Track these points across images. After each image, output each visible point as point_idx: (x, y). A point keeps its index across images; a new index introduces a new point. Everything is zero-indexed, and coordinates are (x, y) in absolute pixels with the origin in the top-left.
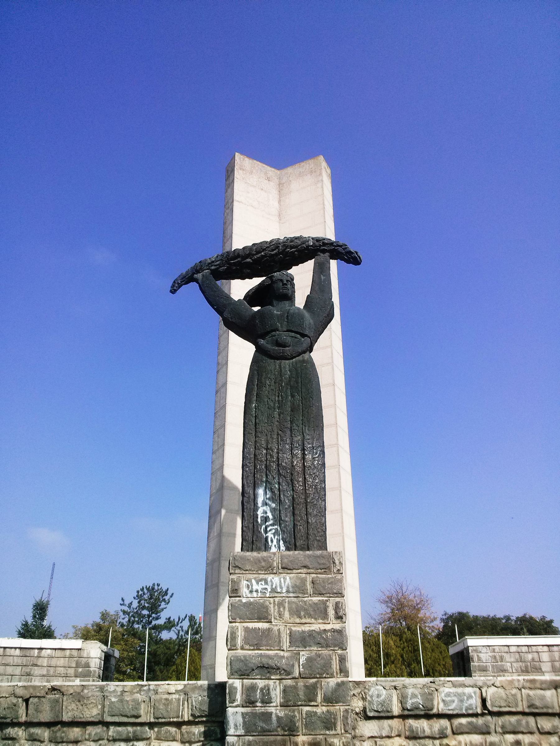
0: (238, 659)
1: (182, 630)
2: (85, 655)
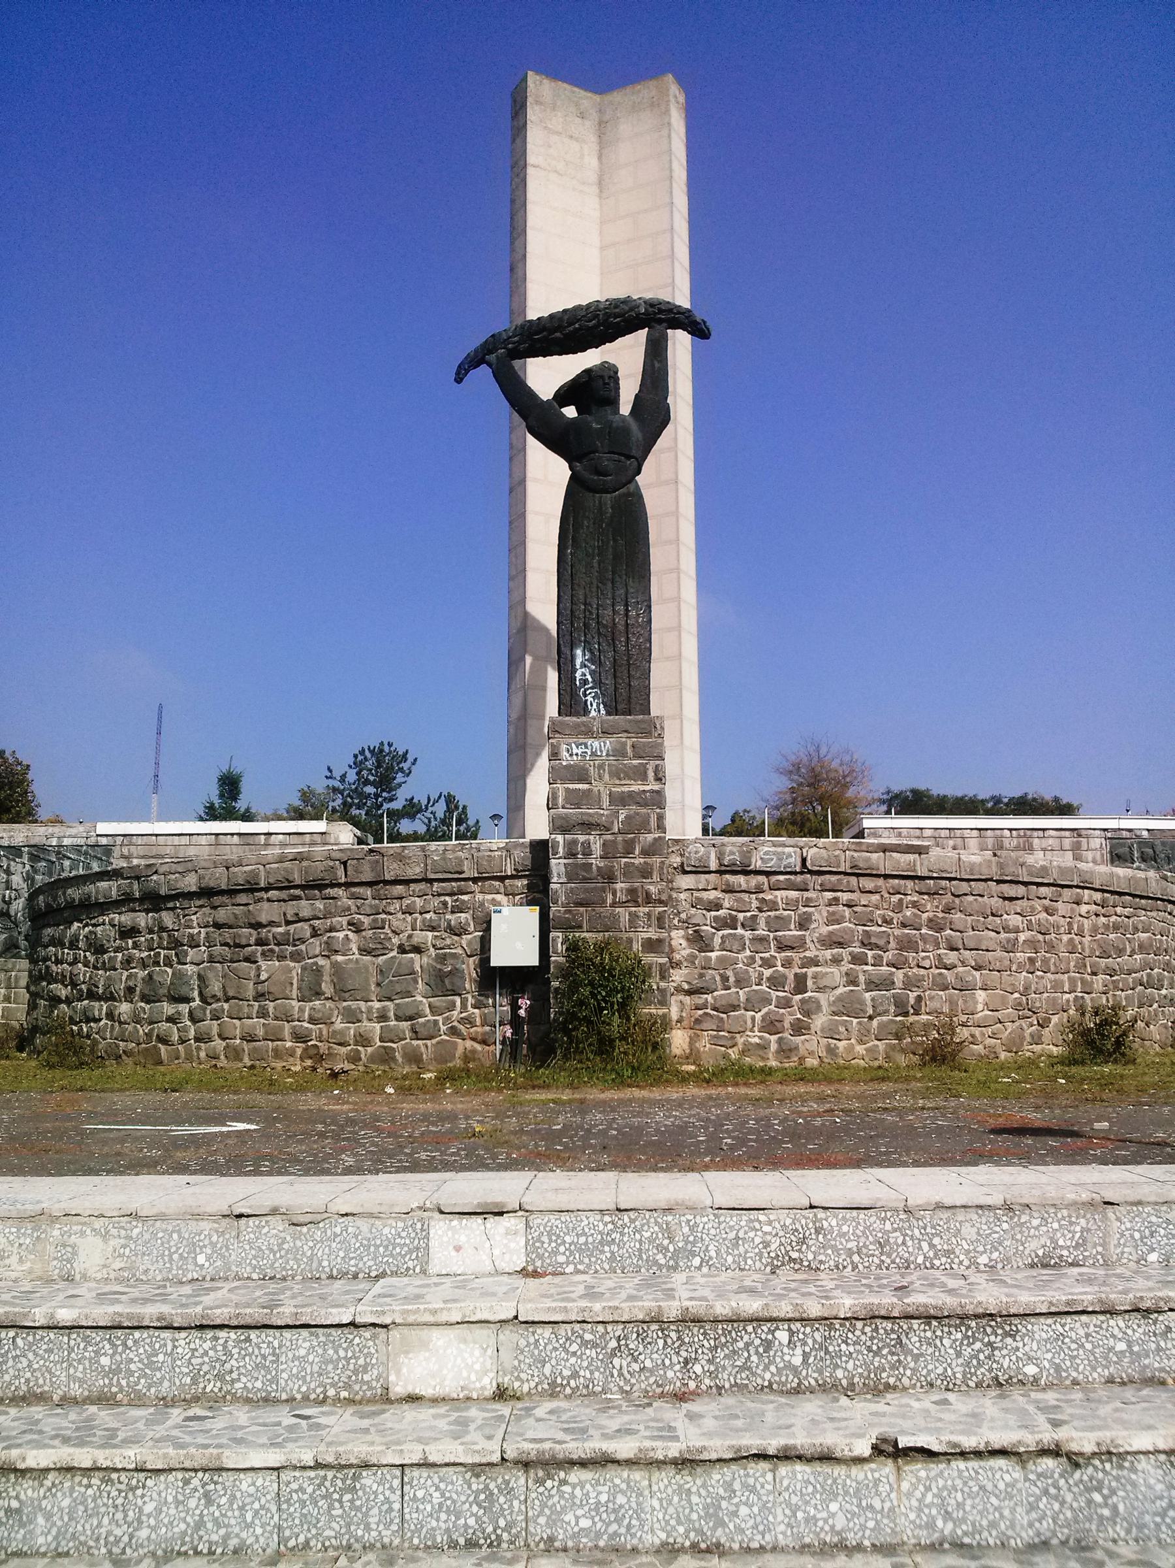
0: (560, 817)
1: (435, 819)
2: (332, 841)
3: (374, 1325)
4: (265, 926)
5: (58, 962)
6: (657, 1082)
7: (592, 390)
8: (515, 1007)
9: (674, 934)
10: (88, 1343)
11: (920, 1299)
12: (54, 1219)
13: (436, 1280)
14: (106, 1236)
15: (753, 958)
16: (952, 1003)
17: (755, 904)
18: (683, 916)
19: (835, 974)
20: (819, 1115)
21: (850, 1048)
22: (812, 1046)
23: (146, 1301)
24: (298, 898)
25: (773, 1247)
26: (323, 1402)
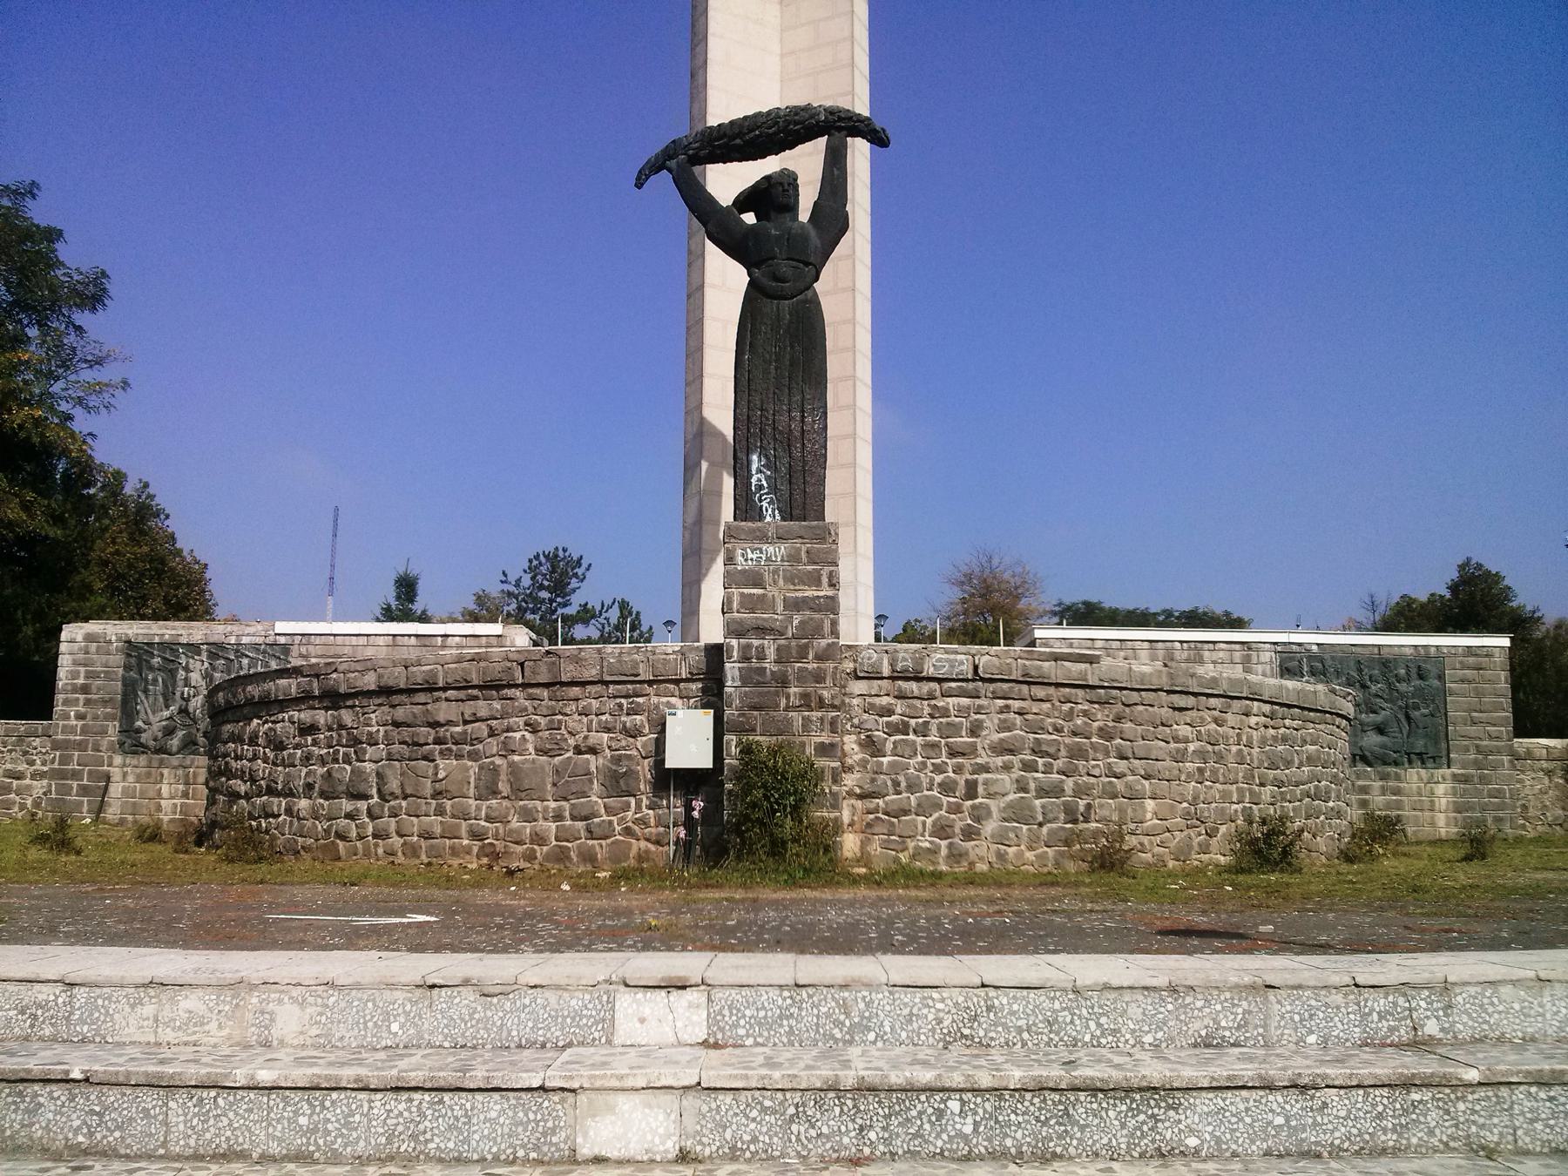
3: (563, 1089)
4: (443, 725)
5: (237, 758)
6: (830, 883)
7: (771, 197)
8: (689, 808)
9: (846, 738)
10: (287, 1104)
11: (1088, 1073)
12: (253, 987)
13: (620, 1050)
14: (302, 1004)
15: (924, 764)
16: (1122, 811)
17: (927, 710)
18: (856, 721)
19: (1006, 780)
20: (989, 915)
21: (1020, 855)
22: (982, 851)
23: (343, 1064)
24: (476, 698)
25: (946, 1023)
26: (513, 1162)
